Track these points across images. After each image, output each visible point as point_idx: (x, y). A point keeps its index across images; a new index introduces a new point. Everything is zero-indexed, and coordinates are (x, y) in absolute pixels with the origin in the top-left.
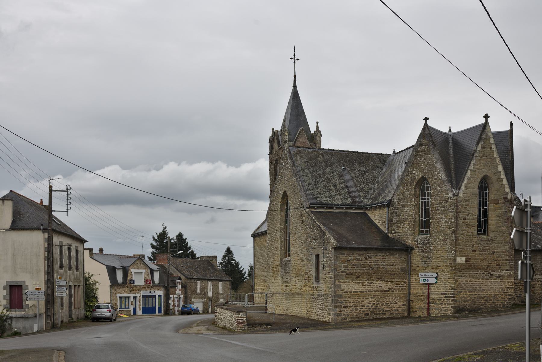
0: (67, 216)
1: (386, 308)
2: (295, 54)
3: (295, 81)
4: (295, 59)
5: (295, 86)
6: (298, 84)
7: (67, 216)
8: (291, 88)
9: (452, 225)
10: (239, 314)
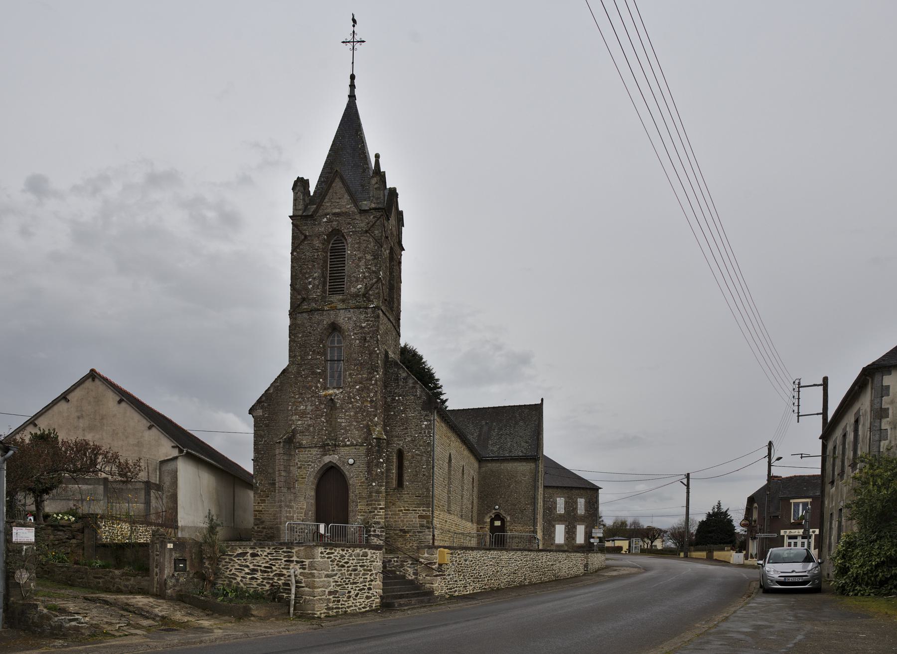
0: (798, 422)
1: (361, 475)
2: (354, 32)
3: (352, 86)
4: (354, 42)
5: (352, 97)
6: (357, 92)
7: (798, 422)
8: (346, 100)
9: (516, 573)
10: (129, 580)
